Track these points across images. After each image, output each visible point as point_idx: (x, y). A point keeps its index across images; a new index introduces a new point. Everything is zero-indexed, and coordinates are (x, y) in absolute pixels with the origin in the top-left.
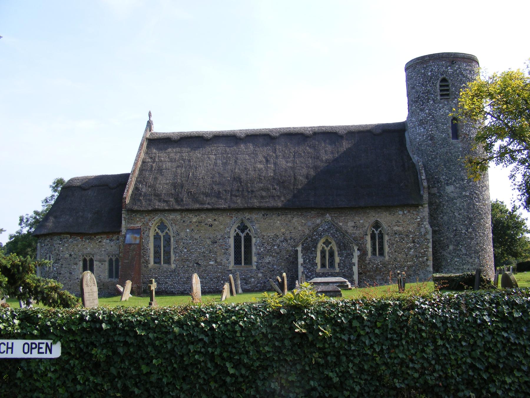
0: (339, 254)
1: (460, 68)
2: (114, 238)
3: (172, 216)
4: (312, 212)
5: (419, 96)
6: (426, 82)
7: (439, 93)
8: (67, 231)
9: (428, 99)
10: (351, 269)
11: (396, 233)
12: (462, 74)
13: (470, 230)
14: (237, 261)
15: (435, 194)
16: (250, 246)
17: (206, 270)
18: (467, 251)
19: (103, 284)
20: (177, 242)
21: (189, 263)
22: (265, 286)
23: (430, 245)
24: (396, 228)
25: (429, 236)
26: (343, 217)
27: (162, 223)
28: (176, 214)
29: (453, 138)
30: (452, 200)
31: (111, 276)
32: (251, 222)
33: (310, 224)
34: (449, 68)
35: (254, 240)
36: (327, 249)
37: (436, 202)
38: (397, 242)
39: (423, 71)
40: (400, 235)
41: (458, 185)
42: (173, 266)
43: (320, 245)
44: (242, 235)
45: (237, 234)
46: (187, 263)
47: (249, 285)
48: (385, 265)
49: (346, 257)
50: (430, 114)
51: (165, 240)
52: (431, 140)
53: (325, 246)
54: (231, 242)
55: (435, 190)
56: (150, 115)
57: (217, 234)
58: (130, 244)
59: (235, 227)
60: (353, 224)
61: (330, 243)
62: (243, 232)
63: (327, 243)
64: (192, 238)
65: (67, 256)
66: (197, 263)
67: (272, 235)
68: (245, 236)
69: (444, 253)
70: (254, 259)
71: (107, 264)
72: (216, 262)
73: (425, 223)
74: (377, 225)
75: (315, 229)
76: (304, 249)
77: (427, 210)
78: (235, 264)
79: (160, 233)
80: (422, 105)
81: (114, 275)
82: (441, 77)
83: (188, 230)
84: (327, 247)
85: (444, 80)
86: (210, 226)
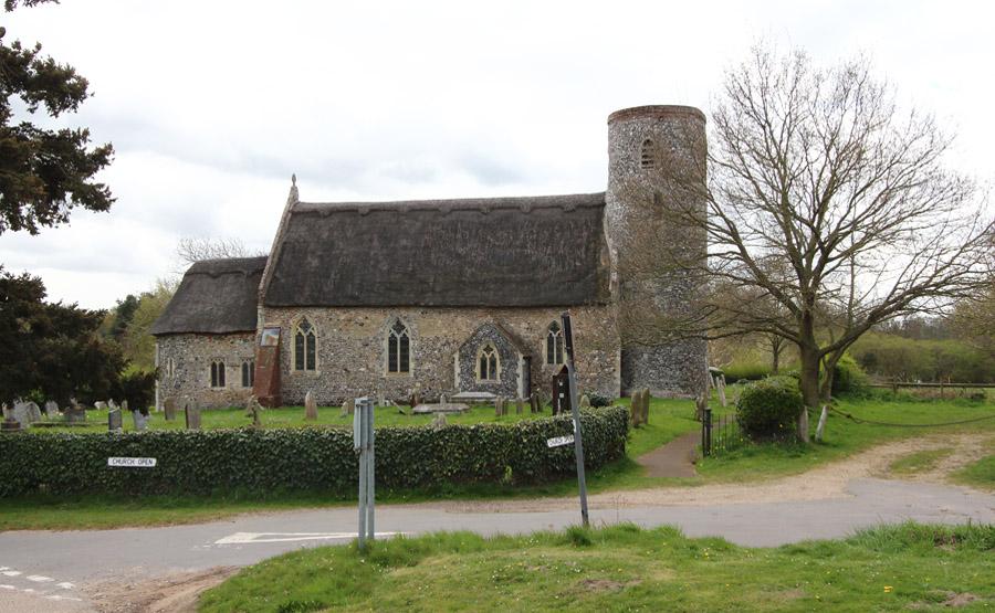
3: (317, 313)
7: (641, 160)
8: (190, 330)
10: (515, 381)
14: (392, 368)
31: (245, 384)
35: (411, 343)
36: (488, 357)
42: (318, 373)
43: (480, 352)
44: (398, 337)
45: (393, 335)
46: (335, 369)
49: (509, 367)
51: (401, 342)
56: (294, 179)
57: (369, 335)
59: (390, 327)
63: (488, 349)
64: (340, 339)
65: (192, 359)
67: (432, 337)
69: (637, 363)
70: (412, 365)
71: (240, 369)
76: (462, 356)
78: (390, 370)
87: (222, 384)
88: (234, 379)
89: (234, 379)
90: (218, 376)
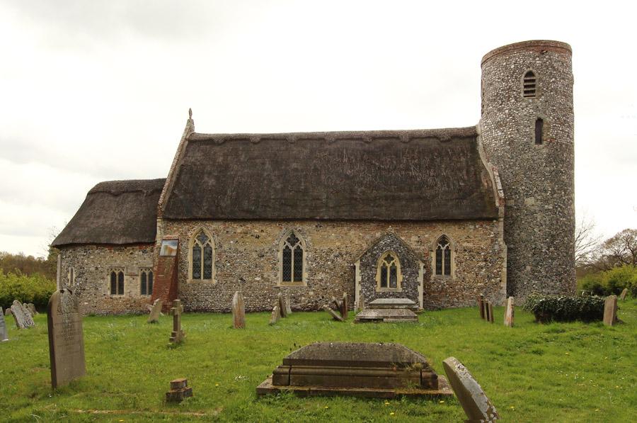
0: (402, 272)
1: (550, 59)
2: (148, 249)
3: (215, 225)
4: (372, 224)
5: (498, 93)
6: (508, 76)
7: (523, 89)
9: (509, 97)
10: (415, 289)
11: (465, 250)
12: (553, 67)
13: (552, 249)
14: (286, 278)
15: (511, 207)
16: (301, 261)
17: (250, 287)
18: (547, 272)
19: (135, 302)
20: (220, 255)
21: (232, 278)
22: (316, 305)
23: (505, 264)
24: (465, 244)
25: (504, 255)
26: (405, 230)
27: (202, 232)
28: (219, 223)
29: (536, 143)
30: (532, 214)
32: (303, 234)
33: (368, 238)
34: (538, 59)
35: (305, 254)
36: (389, 266)
37: (512, 216)
38: (466, 260)
39: (504, 64)
40: (470, 252)
41: (539, 198)
42: (214, 282)
43: (381, 261)
44: (293, 249)
45: (287, 247)
47: (299, 304)
48: (451, 285)
49: (410, 276)
50: (510, 115)
51: (205, 253)
52: (509, 144)
53: (386, 262)
54: (280, 255)
55: (511, 203)
57: (265, 247)
58: (165, 257)
59: (284, 239)
60: (417, 239)
61: (393, 259)
62: (293, 245)
64: (236, 251)
65: (93, 269)
66: (242, 279)
67: (326, 248)
68: (295, 250)
69: (519, 274)
70: (305, 275)
71: (139, 281)
72: (262, 277)
73: (499, 239)
74: (443, 240)
75: (376, 243)
76: (362, 265)
77: (501, 224)
79: (200, 245)
80: (501, 105)
81: (117, 291)
82: (527, 70)
83: (231, 242)
84: (443, 246)
85: (530, 74)
86: (256, 237)
87: (121, 292)
88: (132, 288)
89: (132, 288)
90: (117, 284)
